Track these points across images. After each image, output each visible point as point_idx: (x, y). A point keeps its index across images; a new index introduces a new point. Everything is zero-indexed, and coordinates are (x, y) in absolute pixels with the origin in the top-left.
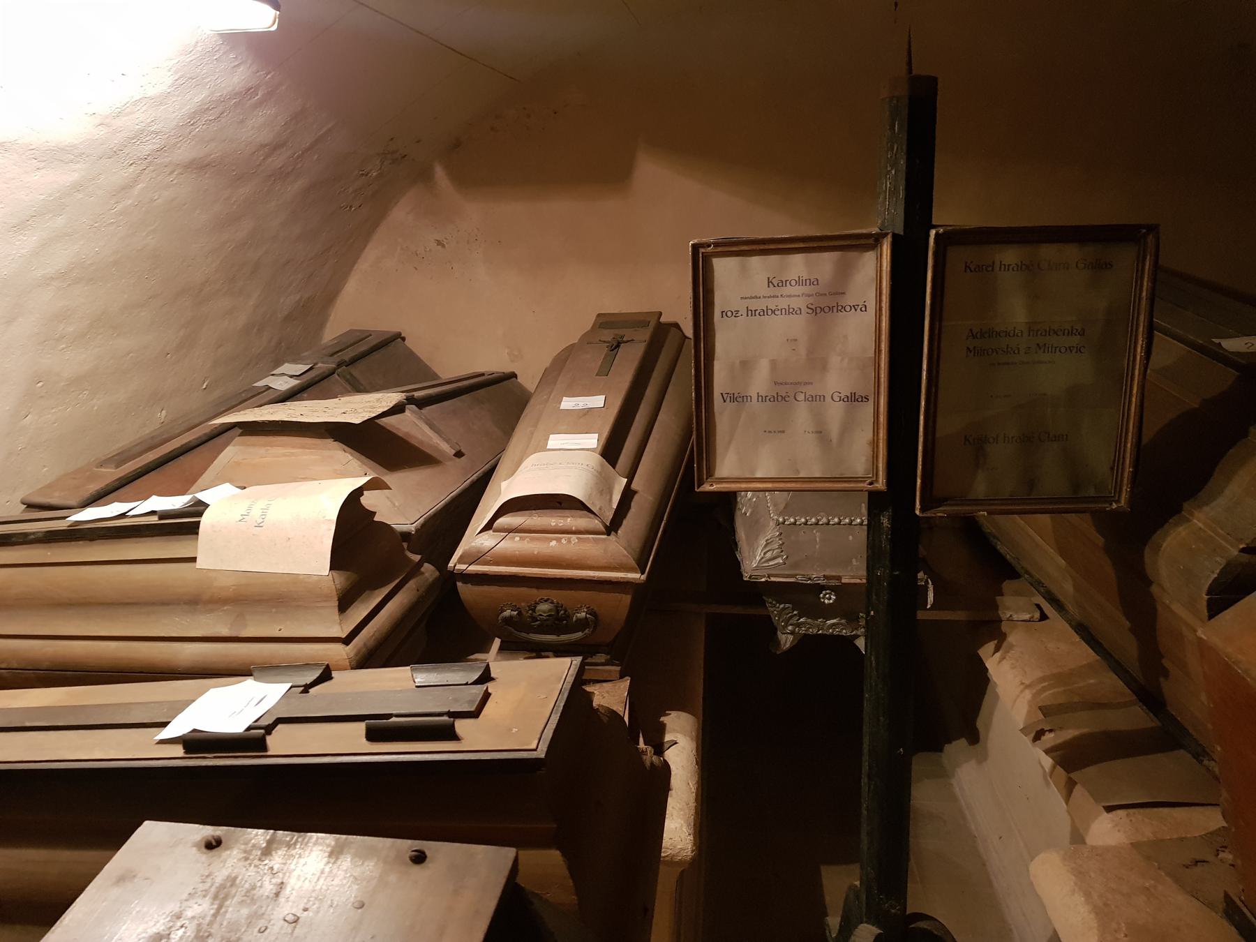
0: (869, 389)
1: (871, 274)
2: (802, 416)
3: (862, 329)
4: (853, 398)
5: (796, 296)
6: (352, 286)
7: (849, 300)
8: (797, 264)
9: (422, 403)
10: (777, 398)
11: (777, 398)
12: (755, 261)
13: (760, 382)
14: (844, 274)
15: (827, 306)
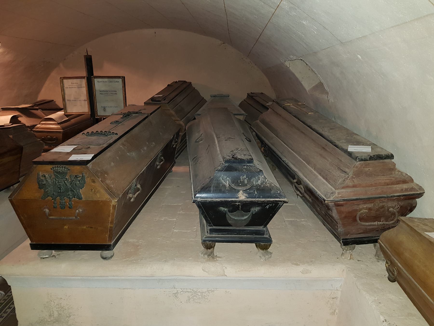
1: (84, 82)
3: (84, 90)
4: (85, 100)
6: (43, 90)
9: (43, 109)
12: (69, 80)
13: (72, 98)
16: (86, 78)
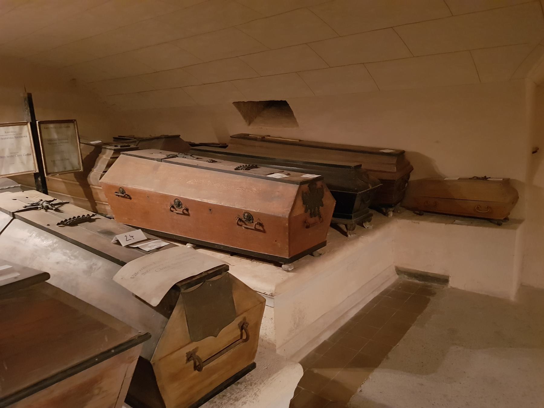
0: (30, 152)
1: (27, 130)
2: (17, 159)
4: (28, 155)
5: (12, 135)
7: (23, 135)
8: (11, 128)
10: (12, 156)
11: (12, 156)
13: (7, 153)
14: (21, 130)
15: (19, 136)
16: (29, 125)
